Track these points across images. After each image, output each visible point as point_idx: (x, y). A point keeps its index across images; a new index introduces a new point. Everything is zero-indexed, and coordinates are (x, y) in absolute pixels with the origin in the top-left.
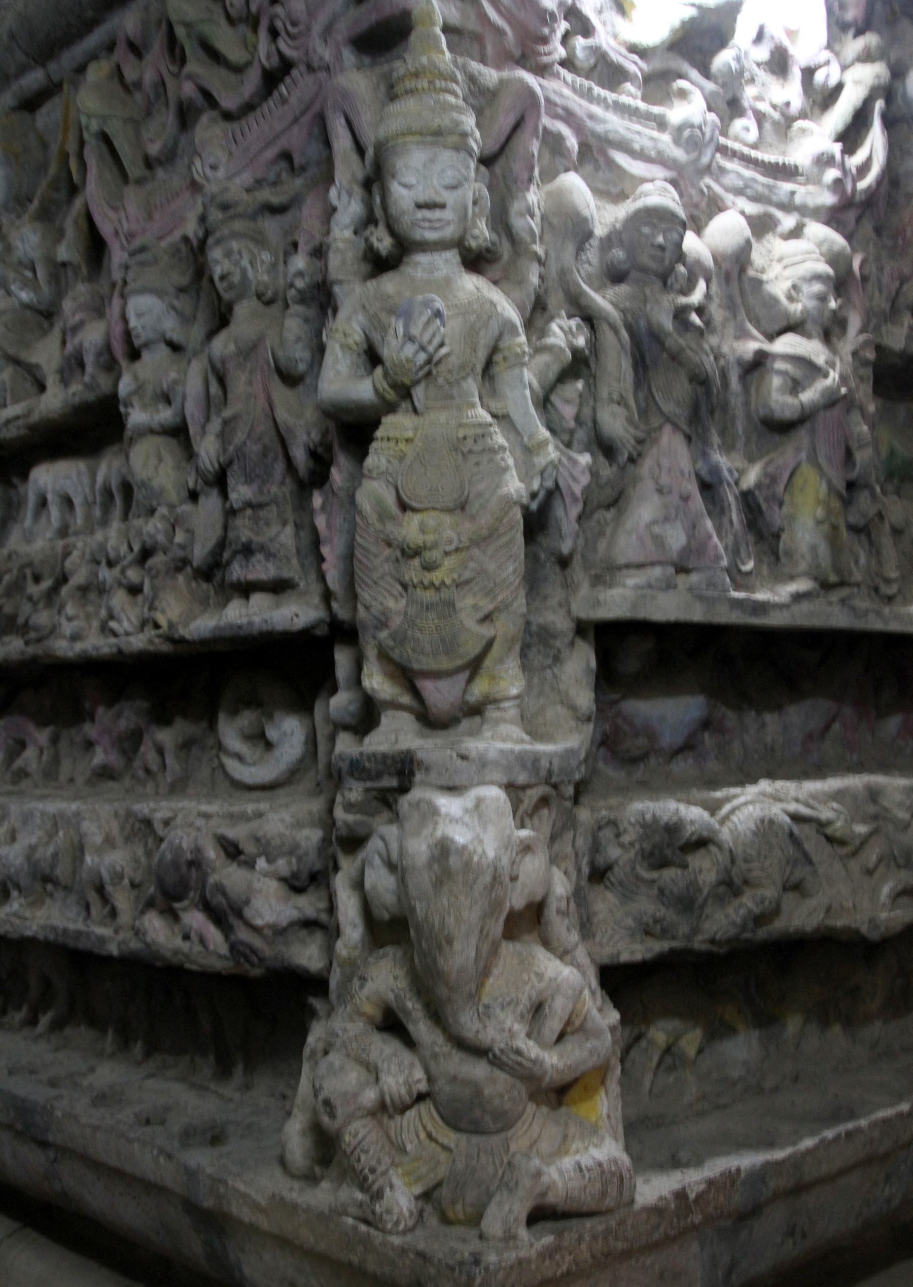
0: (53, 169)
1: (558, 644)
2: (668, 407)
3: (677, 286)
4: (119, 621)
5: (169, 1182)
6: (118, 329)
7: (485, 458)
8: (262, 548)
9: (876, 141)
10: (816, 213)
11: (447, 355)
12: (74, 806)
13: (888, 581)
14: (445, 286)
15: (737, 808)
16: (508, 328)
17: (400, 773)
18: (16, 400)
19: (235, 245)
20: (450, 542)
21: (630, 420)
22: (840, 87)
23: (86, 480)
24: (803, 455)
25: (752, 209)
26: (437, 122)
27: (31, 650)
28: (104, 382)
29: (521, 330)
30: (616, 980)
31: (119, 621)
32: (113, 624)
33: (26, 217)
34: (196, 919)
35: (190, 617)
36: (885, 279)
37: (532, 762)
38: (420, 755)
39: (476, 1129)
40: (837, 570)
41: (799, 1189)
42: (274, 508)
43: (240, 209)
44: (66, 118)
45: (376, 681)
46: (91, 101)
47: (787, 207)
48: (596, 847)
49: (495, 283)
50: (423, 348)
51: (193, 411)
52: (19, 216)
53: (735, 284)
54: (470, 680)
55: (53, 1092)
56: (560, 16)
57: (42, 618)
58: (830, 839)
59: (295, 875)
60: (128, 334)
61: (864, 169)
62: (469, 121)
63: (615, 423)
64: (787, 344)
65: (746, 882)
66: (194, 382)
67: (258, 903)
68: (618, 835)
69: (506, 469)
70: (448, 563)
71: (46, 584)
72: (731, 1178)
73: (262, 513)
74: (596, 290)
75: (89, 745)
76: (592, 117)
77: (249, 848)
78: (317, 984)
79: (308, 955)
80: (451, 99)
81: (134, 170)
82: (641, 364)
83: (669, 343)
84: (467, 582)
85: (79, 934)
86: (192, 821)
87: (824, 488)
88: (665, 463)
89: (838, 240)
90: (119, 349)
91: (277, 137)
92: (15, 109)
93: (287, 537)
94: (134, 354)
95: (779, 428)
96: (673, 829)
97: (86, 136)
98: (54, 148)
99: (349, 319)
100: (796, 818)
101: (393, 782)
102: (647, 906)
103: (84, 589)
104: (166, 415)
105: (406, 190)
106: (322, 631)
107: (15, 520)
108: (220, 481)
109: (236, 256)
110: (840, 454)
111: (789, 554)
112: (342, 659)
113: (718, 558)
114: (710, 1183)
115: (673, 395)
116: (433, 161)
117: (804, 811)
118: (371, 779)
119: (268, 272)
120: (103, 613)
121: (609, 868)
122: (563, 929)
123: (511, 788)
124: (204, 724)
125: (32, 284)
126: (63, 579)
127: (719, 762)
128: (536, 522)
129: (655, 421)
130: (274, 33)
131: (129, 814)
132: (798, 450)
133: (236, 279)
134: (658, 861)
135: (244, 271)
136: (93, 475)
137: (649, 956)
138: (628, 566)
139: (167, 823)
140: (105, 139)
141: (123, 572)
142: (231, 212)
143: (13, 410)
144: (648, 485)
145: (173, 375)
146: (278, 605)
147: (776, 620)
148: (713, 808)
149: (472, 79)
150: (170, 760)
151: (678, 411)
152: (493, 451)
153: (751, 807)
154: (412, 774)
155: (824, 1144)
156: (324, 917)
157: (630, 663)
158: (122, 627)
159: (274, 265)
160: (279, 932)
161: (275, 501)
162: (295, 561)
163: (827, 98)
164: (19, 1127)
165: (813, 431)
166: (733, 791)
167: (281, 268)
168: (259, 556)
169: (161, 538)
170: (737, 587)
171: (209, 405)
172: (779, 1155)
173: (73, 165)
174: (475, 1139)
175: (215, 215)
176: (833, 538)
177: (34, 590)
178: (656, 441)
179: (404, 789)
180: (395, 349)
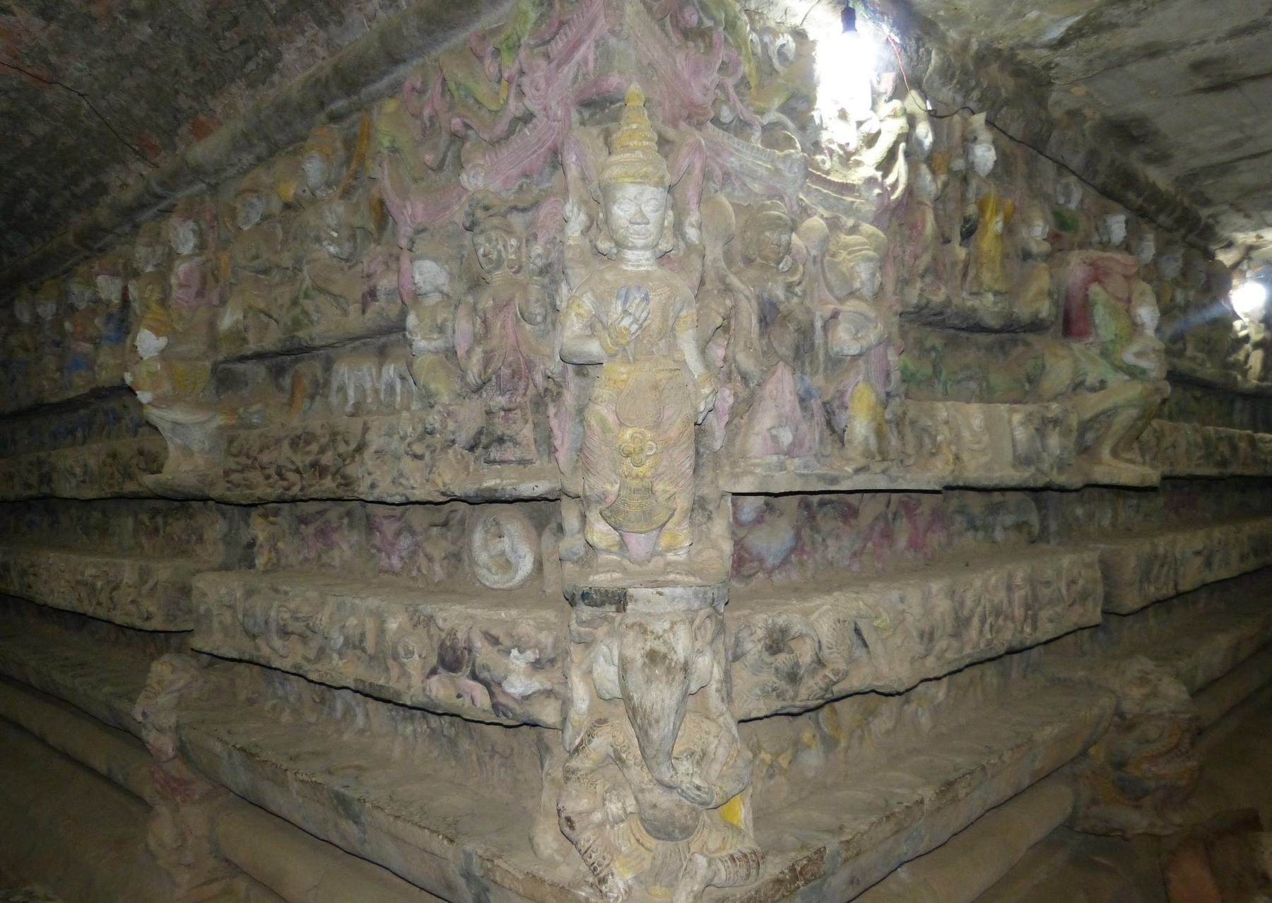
4: (408, 479)
9: (900, 167)
11: (649, 325)
13: (909, 456)
19: (493, 234)
22: (879, 133)
24: (861, 378)
36: (907, 258)
39: (669, 837)
42: (518, 411)
48: (738, 642)
53: (819, 266)
61: (894, 186)
63: (746, 362)
66: (464, 328)
77: (506, 642)
82: (764, 322)
84: (659, 475)
93: (526, 432)
102: (768, 678)
109: (494, 243)
115: (785, 340)
119: (515, 252)
120: (395, 474)
121: (743, 654)
132: (858, 374)
133: (494, 256)
135: (499, 251)
141: (409, 445)
142: (491, 212)
159: (519, 248)
161: (519, 407)
162: (533, 447)
163: (871, 140)
166: (818, 602)
167: (524, 250)
168: (508, 443)
169: (437, 426)
171: (477, 340)
175: (480, 214)
176: (880, 434)
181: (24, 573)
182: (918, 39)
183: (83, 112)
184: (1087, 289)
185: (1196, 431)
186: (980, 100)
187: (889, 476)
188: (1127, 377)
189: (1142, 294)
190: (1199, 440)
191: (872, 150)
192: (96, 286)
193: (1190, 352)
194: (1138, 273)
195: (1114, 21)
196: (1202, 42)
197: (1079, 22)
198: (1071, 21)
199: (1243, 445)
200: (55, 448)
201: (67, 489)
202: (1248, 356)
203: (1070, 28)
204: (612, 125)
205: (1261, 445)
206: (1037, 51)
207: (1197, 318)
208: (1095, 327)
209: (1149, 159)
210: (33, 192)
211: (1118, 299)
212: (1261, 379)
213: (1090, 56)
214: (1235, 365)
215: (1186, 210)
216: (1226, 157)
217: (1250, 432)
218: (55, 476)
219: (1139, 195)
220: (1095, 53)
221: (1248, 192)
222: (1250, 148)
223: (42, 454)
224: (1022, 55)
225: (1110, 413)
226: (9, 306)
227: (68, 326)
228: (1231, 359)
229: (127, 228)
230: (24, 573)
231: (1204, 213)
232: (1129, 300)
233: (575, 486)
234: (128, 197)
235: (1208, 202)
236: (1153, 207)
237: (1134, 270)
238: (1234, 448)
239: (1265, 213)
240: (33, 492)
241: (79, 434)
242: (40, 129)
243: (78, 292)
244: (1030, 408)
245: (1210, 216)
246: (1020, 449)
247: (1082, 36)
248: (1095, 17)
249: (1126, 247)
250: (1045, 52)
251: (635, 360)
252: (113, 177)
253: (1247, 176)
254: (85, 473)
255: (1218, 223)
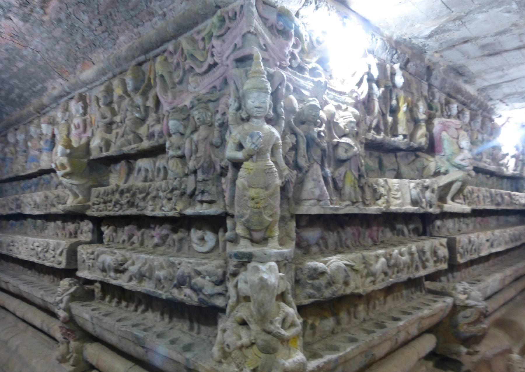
0: (146, 81)
1: (286, 220)
2: (315, 158)
3: (318, 125)
5: (180, 361)
6: (165, 128)
7: (271, 175)
8: (207, 192)
10: (350, 104)
12: (152, 257)
14: (261, 128)
15: (331, 263)
16: (278, 139)
17: (248, 258)
18: (135, 143)
20: (262, 196)
21: (306, 162)
23: (152, 165)
25: (336, 104)
26: (261, 86)
27: (139, 213)
28: (161, 141)
29: (280, 139)
30: (301, 309)
31: (165, 207)
32: (163, 208)
33: (138, 94)
34: (188, 291)
35: (186, 208)
37: (281, 254)
38: (254, 253)
39: (268, 353)
40: (356, 199)
41: (346, 361)
43: (202, 101)
44: (150, 68)
45: (240, 230)
46: (159, 67)
47: (343, 103)
49: (273, 126)
50: (256, 146)
51: (187, 153)
52: (136, 93)
54: (265, 232)
55: (145, 333)
56: (289, 55)
57: (141, 204)
58: (354, 270)
59: (216, 281)
60: (168, 129)
62: (269, 85)
64: (344, 140)
65: (334, 283)
67: (206, 288)
68: (302, 271)
69: (276, 177)
70: (262, 202)
71: (144, 195)
72: (330, 361)
73: (207, 182)
74: (297, 126)
75: (153, 237)
76: (296, 80)
78: (223, 310)
79: (219, 302)
80: (264, 79)
81: (170, 86)
82: (308, 146)
83: (316, 141)
85: (154, 292)
86: (186, 264)
87: (353, 178)
88: (315, 172)
89: (357, 112)
90: (165, 132)
91: (213, 82)
92: (136, 65)
94: (170, 135)
95: (341, 162)
96: (315, 269)
97: (157, 75)
98: (147, 77)
99: (219, 119)
100: (346, 265)
101: (246, 260)
103: (155, 197)
104: (179, 153)
105: (251, 102)
106: (223, 215)
107: (132, 173)
108: (195, 172)
110: (357, 168)
111: (343, 194)
112: (229, 223)
113: (327, 197)
114: (325, 363)
115: (317, 154)
116: (259, 96)
117: (348, 263)
118: (240, 259)
122: (290, 297)
123: (277, 262)
124: (187, 234)
125: (139, 112)
126: (148, 194)
127: (325, 250)
128: (283, 189)
129: (312, 161)
130: (213, 55)
131: (169, 261)
134: (312, 278)
136: (155, 163)
137: (309, 303)
138: (305, 200)
139: (179, 264)
140: (162, 76)
142: (200, 101)
143: (133, 146)
144: (310, 178)
145: (181, 142)
146: (211, 208)
147: (341, 212)
148: (325, 263)
149: (268, 72)
150: (176, 243)
151: (318, 159)
152: (273, 172)
153: (335, 262)
154: (252, 258)
155: (352, 350)
156: (224, 292)
157: (303, 223)
158: (167, 210)
160: (211, 296)
164: (136, 342)
165: (350, 163)
166: (330, 258)
168: (206, 194)
169: (178, 186)
170: (332, 204)
172: (341, 354)
173: (152, 81)
174: (268, 355)
177: (141, 196)
178: (313, 167)
179: (249, 262)
180: (248, 144)
181: (9, 245)
182: (373, 35)
183: (38, 58)
184: (441, 134)
185: (487, 191)
186: (397, 58)
187: (359, 208)
188: (457, 169)
189: (463, 136)
190: (488, 195)
191: (375, 64)
192: (41, 128)
193: (484, 159)
194: (461, 127)
195: (450, 28)
196: (485, 37)
197: (436, 29)
198: (433, 28)
199: (506, 197)
200: (23, 194)
201: (27, 211)
202: (508, 161)
203: (433, 31)
204: (248, 68)
205: (514, 197)
206: (420, 40)
207: (489, 146)
208: (444, 149)
209: (466, 82)
210: (17, 91)
211: (454, 138)
212: (515, 170)
213: (441, 42)
214: (502, 165)
215: (482, 103)
216: (499, 81)
217: (509, 192)
218: (22, 205)
219: (463, 96)
220: (443, 41)
221: (507, 96)
222: (507, 78)
223: (17, 196)
224: (414, 41)
225: (451, 184)
226: (5, 136)
227: (29, 144)
228: (501, 162)
229: (54, 105)
230: (9, 245)
231: (490, 103)
232: (458, 138)
233: (230, 212)
234: (56, 93)
235: (491, 99)
236: (469, 101)
237: (460, 126)
238: (502, 198)
239: (514, 104)
240: (13, 212)
241: (33, 188)
242: (20, 65)
243: (32, 129)
244: (418, 181)
245: (492, 105)
246: (413, 197)
247: (437, 34)
248: (442, 27)
249: (458, 117)
250: (422, 40)
251: (257, 161)
252: (49, 84)
253: (506, 89)
254: (35, 204)
255: (495, 107)
